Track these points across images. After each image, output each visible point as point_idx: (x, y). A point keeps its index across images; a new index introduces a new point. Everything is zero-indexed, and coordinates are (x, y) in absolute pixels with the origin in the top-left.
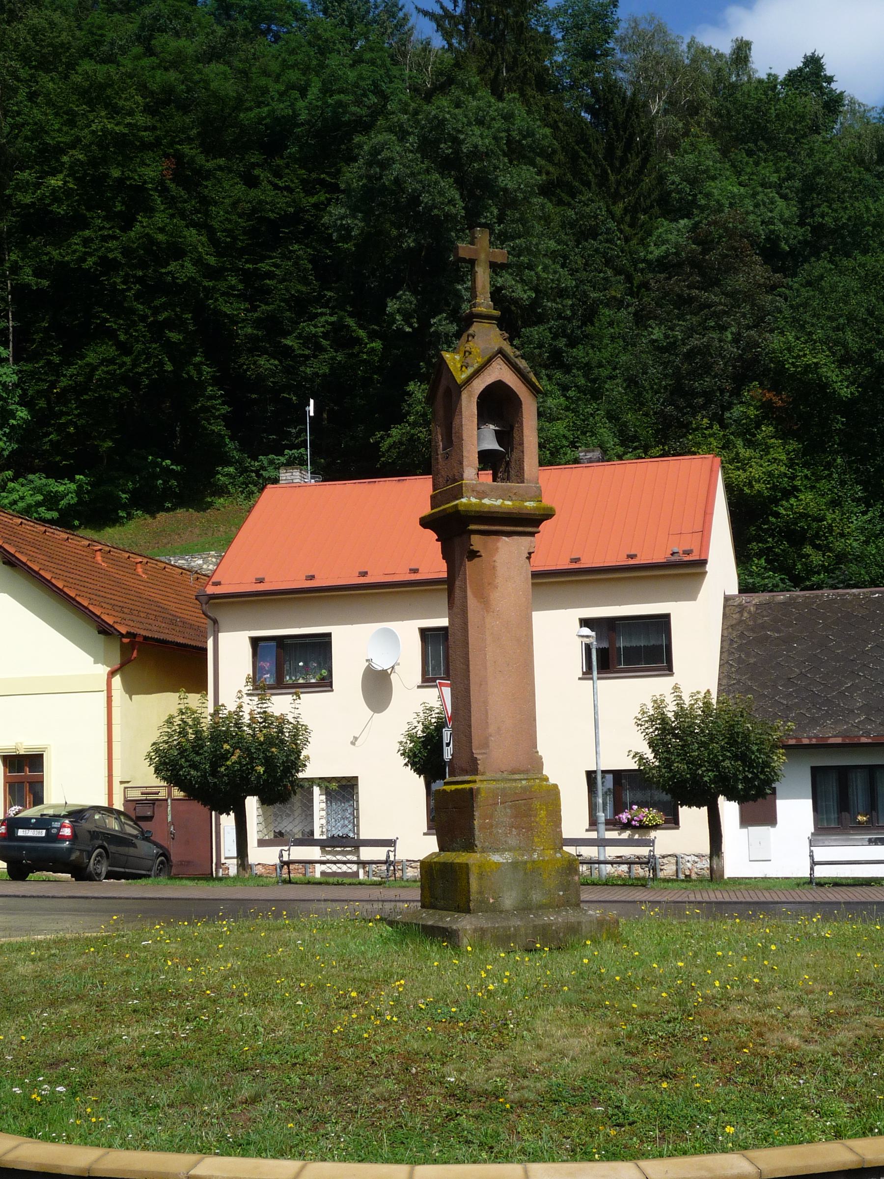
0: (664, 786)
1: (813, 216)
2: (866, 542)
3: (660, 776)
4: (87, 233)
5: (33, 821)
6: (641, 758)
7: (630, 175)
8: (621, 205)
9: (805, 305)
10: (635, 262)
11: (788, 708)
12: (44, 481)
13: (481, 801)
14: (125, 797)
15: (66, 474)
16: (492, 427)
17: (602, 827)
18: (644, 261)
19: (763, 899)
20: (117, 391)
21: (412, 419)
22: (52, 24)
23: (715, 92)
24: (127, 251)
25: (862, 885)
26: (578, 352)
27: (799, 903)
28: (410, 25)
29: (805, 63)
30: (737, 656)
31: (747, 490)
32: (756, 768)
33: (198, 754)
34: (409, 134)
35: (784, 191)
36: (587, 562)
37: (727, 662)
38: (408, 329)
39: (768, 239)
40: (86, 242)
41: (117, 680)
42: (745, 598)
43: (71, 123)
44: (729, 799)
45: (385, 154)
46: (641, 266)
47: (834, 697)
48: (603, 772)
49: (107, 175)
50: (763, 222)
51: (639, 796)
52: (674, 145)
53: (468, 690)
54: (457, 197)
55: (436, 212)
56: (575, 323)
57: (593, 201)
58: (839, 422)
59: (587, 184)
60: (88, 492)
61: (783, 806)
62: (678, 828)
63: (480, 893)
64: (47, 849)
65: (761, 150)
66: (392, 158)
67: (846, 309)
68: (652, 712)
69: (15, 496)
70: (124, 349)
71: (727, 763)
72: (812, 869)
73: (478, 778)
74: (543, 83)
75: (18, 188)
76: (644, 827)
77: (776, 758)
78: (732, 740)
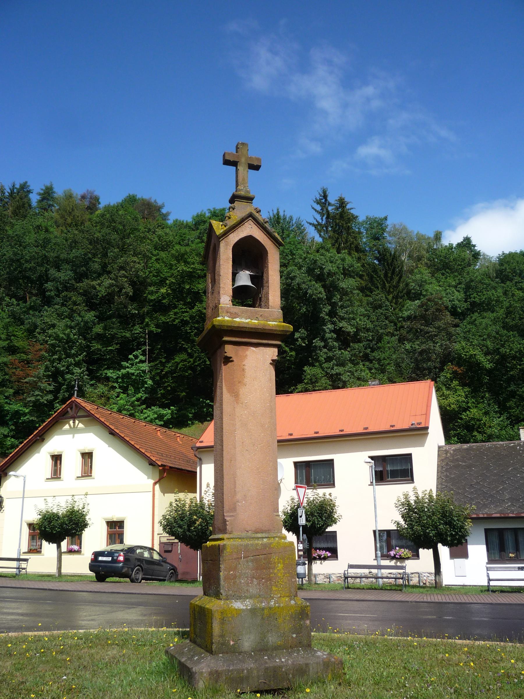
0: (410, 538)
1: (471, 298)
2: (501, 430)
3: (408, 533)
4: (176, 310)
5: (106, 553)
6: (398, 524)
7: (394, 284)
8: (391, 296)
9: (469, 331)
10: (398, 318)
11: (472, 499)
12: (158, 409)
13: (226, 554)
14: (160, 541)
15: (167, 406)
16: (248, 272)
17: (379, 559)
18: (402, 317)
19: (463, 601)
20: (187, 372)
21: (306, 381)
22: (166, 234)
23: (428, 252)
24: (192, 317)
25: (515, 592)
26: (375, 354)
27: (484, 603)
28: (306, 232)
29: (464, 240)
30: (445, 474)
31: (448, 408)
32: (457, 529)
33: (182, 520)
34: (303, 267)
35: (458, 289)
36: (371, 429)
37: (440, 477)
38: (304, 345)
39: (452, 307)
40: (176, 314)
41: (157, 486)
42: (448, 447)
43: (171, 269)
44: (444, 545)
45: (293, 274)
46: (400, 319)
47: (494, 494)
48: (379, 531)
49: (184, 288)
50: (450, 301)
51: (400, 543)
52: (411, 272)
53: (222, 465)
54: (323, 290)
55: (314, 297)
56: (374, 342)
57: (379, 294)
58: (486, 379)
59: (378, 288)
60: (176, 414)
61: (471, 548)
62: (419, 559)
63: (222, 636)
64: (111, 567)
65: (448, 273)
66: (296, 276)
67: (487, 333)
68: (403, 500)
69: (146, 415)
70: (190, 355)
71: (441, 527)
72: (489, 583)
73: (225, 536)
74: (358, 249)
75: (149, 293)
76: (402, 559)
77: (467, 524)
78: (444, 515)
